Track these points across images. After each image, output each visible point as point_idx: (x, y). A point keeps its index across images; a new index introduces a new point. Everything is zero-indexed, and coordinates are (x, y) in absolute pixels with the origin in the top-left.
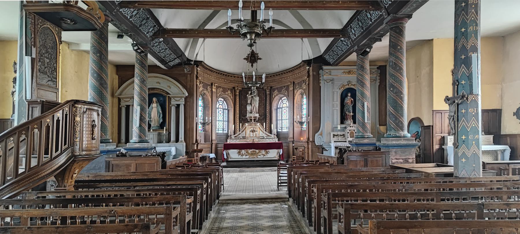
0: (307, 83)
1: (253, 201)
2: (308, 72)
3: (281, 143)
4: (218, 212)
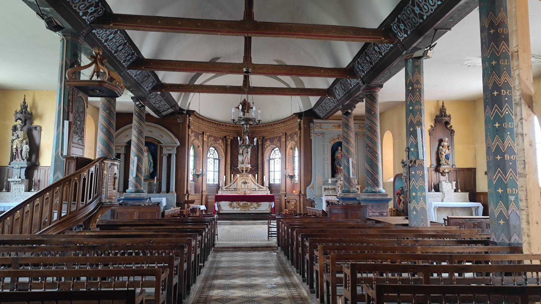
0: (299, 135)
1: (245, 249)
2: (300, 124)
3: (273, 196)
4: (214, 257)
